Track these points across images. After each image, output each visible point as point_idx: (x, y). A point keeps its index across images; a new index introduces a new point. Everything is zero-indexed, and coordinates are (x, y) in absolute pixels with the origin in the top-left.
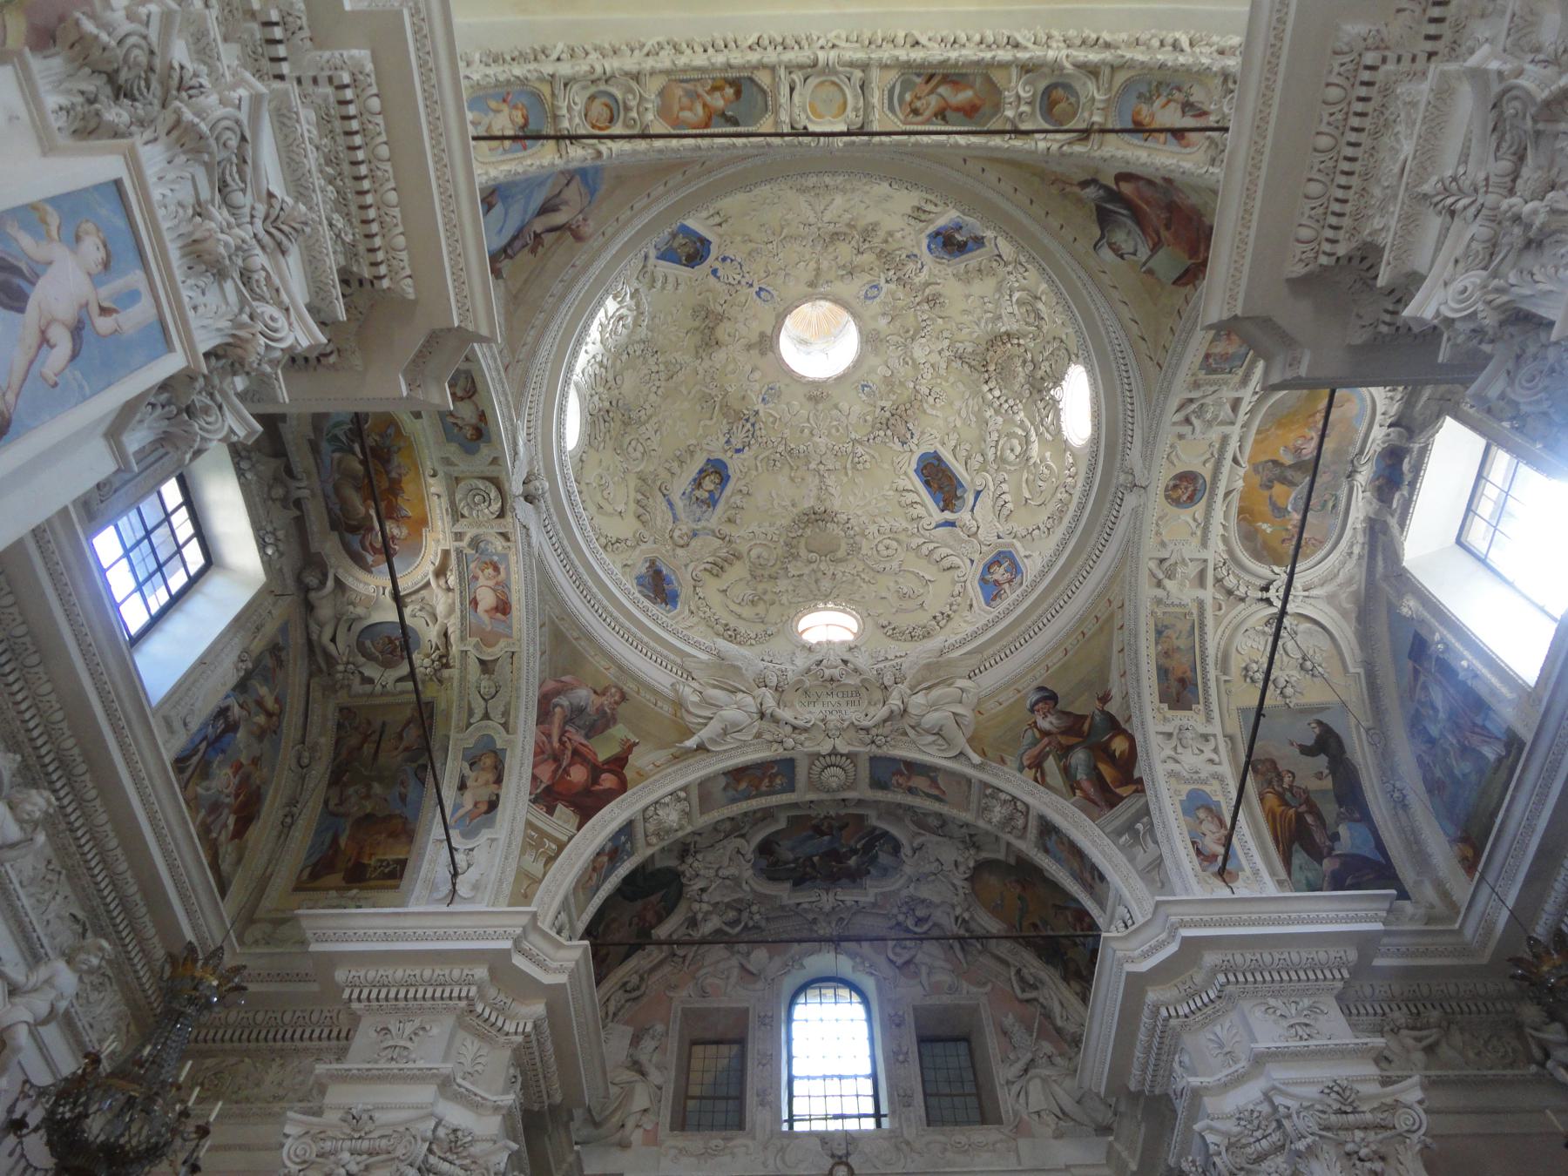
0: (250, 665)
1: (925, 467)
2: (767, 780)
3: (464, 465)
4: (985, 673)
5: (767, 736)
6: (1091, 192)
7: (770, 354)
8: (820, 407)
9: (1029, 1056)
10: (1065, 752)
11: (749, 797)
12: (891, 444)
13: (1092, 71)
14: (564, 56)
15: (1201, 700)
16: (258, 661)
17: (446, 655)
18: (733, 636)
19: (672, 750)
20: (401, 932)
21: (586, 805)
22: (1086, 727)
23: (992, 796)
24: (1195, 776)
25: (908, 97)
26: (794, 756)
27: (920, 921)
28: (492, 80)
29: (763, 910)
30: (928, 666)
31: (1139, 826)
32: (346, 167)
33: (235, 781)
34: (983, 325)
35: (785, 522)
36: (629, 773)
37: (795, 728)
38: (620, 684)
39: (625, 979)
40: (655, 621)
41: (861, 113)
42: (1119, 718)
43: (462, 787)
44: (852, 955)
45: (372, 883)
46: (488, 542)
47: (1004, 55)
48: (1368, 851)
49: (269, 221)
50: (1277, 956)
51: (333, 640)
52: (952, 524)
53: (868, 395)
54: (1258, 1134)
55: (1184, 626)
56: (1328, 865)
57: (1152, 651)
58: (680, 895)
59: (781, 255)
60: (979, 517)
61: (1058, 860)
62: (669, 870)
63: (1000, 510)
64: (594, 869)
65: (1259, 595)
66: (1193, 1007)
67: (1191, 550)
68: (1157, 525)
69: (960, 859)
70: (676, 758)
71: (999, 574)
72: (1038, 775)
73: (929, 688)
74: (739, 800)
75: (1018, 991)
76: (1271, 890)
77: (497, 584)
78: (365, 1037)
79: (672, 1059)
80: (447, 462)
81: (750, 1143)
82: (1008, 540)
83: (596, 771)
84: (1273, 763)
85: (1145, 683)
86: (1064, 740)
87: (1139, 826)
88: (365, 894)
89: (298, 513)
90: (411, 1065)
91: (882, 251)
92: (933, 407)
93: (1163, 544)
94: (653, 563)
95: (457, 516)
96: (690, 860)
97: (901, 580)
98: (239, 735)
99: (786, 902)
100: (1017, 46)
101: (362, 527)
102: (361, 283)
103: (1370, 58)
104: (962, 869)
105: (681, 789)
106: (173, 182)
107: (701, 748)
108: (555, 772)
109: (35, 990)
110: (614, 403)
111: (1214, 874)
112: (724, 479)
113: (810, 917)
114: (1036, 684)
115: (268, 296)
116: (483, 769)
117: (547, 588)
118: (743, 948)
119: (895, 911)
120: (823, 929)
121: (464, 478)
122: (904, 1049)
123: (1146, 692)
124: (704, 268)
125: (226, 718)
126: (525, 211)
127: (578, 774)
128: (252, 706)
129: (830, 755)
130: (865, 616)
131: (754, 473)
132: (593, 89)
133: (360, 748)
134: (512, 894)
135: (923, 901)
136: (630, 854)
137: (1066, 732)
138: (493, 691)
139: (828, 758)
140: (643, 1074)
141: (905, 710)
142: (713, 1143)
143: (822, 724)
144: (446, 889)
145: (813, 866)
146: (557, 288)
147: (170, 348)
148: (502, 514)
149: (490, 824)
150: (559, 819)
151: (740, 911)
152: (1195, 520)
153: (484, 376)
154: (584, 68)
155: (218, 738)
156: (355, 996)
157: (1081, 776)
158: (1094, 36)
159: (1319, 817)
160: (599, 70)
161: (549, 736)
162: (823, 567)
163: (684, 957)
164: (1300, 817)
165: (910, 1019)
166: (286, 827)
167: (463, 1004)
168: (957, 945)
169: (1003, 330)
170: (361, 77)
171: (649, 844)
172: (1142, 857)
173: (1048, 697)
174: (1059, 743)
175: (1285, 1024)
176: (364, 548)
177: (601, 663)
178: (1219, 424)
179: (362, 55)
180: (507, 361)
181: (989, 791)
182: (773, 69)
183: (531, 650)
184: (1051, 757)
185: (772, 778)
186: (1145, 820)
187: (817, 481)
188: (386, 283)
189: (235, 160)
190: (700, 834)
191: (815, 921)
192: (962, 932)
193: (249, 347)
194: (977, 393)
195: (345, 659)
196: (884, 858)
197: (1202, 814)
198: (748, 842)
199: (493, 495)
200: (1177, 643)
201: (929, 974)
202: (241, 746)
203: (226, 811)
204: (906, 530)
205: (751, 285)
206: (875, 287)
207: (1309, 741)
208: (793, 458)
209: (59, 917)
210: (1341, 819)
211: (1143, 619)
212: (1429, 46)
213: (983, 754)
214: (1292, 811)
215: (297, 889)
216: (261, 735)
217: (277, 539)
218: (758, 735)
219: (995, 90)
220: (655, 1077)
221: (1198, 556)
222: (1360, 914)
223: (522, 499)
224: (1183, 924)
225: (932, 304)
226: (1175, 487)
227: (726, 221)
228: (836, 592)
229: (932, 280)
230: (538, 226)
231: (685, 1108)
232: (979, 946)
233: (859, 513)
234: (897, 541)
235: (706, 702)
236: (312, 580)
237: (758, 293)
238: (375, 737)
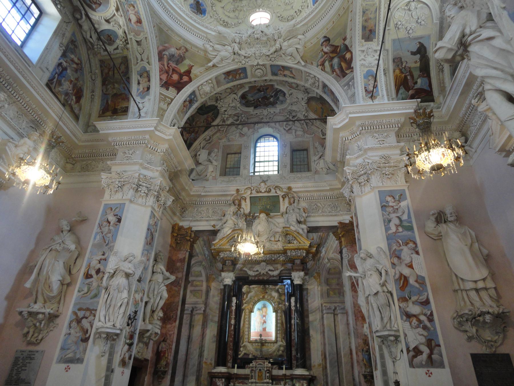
2: (238, 75)
4: (308, 32)
5: (236, 60)
10: (332, 59)
11: (233, 81)
15: (377, 37)
16: (67, 47)
18: (226, 25)
19: (205, 67)
20: (123, 127)
21: (179, 86)
22: (338, 50)
23: (309, 76)
27: (294, 117)
29: (245, 116)
30: (289, 31)
31: (351, 83)
33: (71, 86)
36: (192, 75)
37: (245, 57)
38: (185, 46)
40: (195, 21)
42: (349, 46)
43: (139, 83)
45: (120, 114)
48: (426, 87)
50: (387, 121)
54: (361, 170)
55: (373, 9)
56: (411, 92)
57: (361, 20)
61: (328, 95)
62: (213, 106)
64: (184, 106)
66: (353, 137)
69: (303, 97)
70: (207, 69)
72: (323, 68)
73: (290, 39)
74: (230, 82)
75: (321, 136)
76: (386, 101)
77: (135, 12)
78: (120, 154)
79: (220, 158)
81: (240, 178)
83: (181, 76)
85: (357, 32)
86: (331, 55)
87: (351, 83)
88: (117, 117)
90: (132, 161)
96: (219, 102)
98: (68, 71)
99: (252, 113)
104: (304, 100)
105: (210, 80)
107: (214, 66)
108: (167, 77)
109: (22, 145)
111: (369, 97)
114: (323, 35)
116: (144, 78)
117: (153, 13)
119: (286, 114)
122: (286, 153)
123: (357, 35)
125: (62, 66)
127: (175, 77)
128: (71, 62)
130: (273, 13)
133: (108, 73)
136: (197, 101)
137: (332, 52)
138: (142, 51)
139: (260, 66)
141: (281, 48)
142: (231, 179)
144: (138, 114)
145: (259, 101)
149: (148, 94)
150: (170, 91)
151: (238, 117)
155: (61, 73)
156: (115, 144)
157: (336, 67)
159: (412, 76)
161: (164, 65)
167: (144, 145)
171: (202, 98)
172: (350, 93)
173: (327, 40)
174: (330, 56)
175: (377, 140)
176: (91, 3)
177: (176, 38)
181: (308, 74)
184: (327, 61)
185: (240, 74)
196: (281, 98)
198: (237, 95)
200: (370, 16)
201: (295, 132)
202: (70, 75)
210: (419, 77)
213: (306, 62)
214: (403, 75)
216: (76, 71)
218: (233, 60)
220: (215, 163)
222: (401, 108)
224: (350, 113)
231: (225, 171)
235: (214, 50)
236: (78, 16)
238: (112, 69)
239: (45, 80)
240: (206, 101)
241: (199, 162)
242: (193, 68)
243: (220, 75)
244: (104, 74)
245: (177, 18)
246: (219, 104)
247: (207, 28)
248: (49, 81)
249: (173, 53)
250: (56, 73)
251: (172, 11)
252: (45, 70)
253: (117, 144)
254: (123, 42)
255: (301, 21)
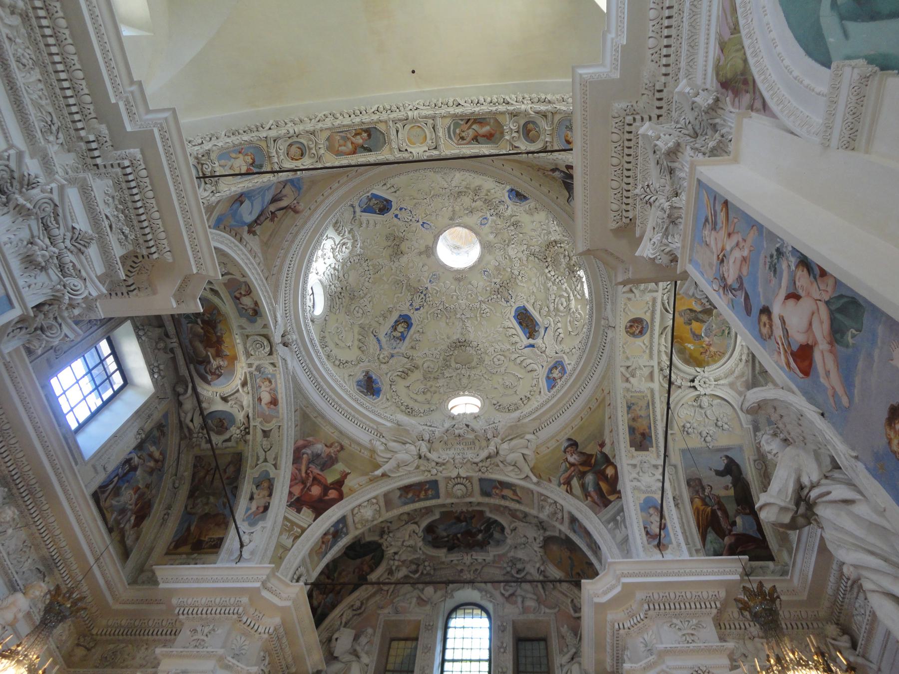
0: (143, 436)
1: (519, 315)
3: (250, 329)
5: (422, 468)
6: (557, 174)
7: (432, 257)
8: (461, 283)
9: (574, 650)
10: (582, 475)
11: (414, 502)
12: (501, 303)
13: (544, 115)
14: (272, 127)
17: (248, 428)
18: (410, 412)
21: (319, 507)
22: (593, 461)
24: (649, 489)
25: (458, 131)
26: (437, 479)
27: (519, 571)
28: (231, 144)
29: (431, 564)
30: (511, 427)
31: (619, 518)
32: (130, 204)
33: (135, 497)
34: (542, 236)
35: (443, 347)
36: (345, 489)
39: (352, 603)
40: (362, 405)
41: (434, 141)
43: (251, 498)
44: (480, 590)
45: (206, 550)
46: (265, 368)
47: (502, 108)
48: (753, 532)
49: (73, 241)
51: (192, 421)
52: (532, 346)
53: (488, 277)
55: (643, 404)
56: (727, 540)
57: (626, 418)
58: (382, 557)
59: (432, 205)
60: (545, 340)
61: (581, 537)
63: (558, 340)
64: (323, 542)
65: (689, 384)
67: (644, 361)
68: (623, 348)
71: (556, 374)
72: (569, 488)
73: (512, 439)
76: (686, 556)
78: (185, 634)
80: (241, 327)
82: (561, 354)
83: (326, 489)
84: (700, 481)
85: (621, 436)
86: (582, 469)
89: (172, 355)
90: (205, 649)
91: (486, 200)
92: (521, 281)
93: (628, 358)
94: (367, 373)
95: (248, 355)
96: (385, 537)
97: (505, 378)
99: (444, 559)
100: (508, 103)
101: (206, 361)
102: (143, 257)
103: (629, 119)
104: (538, 541)
105: (374, 498)
106: (15, 231)
107: (384, 475)
108: (302, 490)
110: (344, 288)
111: (655, 546)
112: (409, 325)
113: (459, 568)
114: (566, 437)
115: (74, 274)
116: (263, 489)
117: (298, 390)
118: (421, 586)
119: (505, 565)
120: (466, 576)
121: (251, 335)
124: (391, 214)
125: (130, 465)
126: (263, 202)
127: (316, 491)
129: (457, 478)
130: (484, 398)
131: (426, 321)
132: (290, 141)
133: (205, 477)
134: (272, 557)
135: (520, 559)
136: (346, 534)
137: (583, 464)
140: (358, 657)
143: (452, 461)
145: (458, 539)
146: (289, 237)
147: (12, 306)
148: (271, 353)
149: (263, 519)
151: (418, 565)
152: (645, 344)
153: (253, 283)
154: (283, 131)
155: (126, 474)
156: (181, 612)
157: (591, 489)
158: (543, 97)
160: (292, 132)
161: (300, 470)
162: (463, 371)
163: (388, 591)
164: (713, 512)
165: (510, 629)
166: (164, 521)
167: (236, 616)
168: (539, 585)
169: (552, 239)
170: (134, 162)
171: (356, 528)
172: (619, 536)
174: (580, 471)
175: (680, 634)
177: (328, 429)
178: (649, 292)
179: (136, 152)
180: (266, 275)
181: (542, 498)
182: (386, 122)
183: (290, 423)
185: (426, 491)
186: (621, 514)
187: (461, 324)
188: (155, 256)
189: (52, 215)
190: (391, 522)
191: (462, 571)
192: (541, 578)
193: (61, 300)
194: (543, 274)
195: (197, 430)
196: (497, 535)
197: (651, 511)
199: (265, 344)
203: (129, 514)
204: (509, 350)
205: (418, 221)
206: (486, 218)
207: (721, 468)
208: (447, 312)
209: (30, 570)
210: (738, 513)
211: (619, 401)
212: (658, 112)
214: (709, 509)
215: (167, 554)
216: (151, 472)
217: (159, 370)
218: (418, 467)
219: (499, 125)
220: (365, 659)
221: (647, 364)
223: (281, 345)
224: (624, 575)
225: (515, 226)
226: (631, 326)
227: (398, 190)
228: (470, 385)
229: (514, 214)
230: (272, 208)
232: (552, 586)
233: (484, 341)
234: (505, 357)
235: (387, 449)
236: (180, 390)
237: (422, 225)
238: (212, 472)
239: (94, 486)
240: (363, 534)
241: (335, 655)
242: (348, 477)
243: (392, 491)
244: (196, 480)
245: (334, 400)
246: (385, 541)
247: (379, 415)
248: (100, 487)
249: (319, 452)
250: (117, 475)
251: (328, 390)
252: (100, 469)
253: (185, 612)
254: (241, 431)
255: (531, 413)
